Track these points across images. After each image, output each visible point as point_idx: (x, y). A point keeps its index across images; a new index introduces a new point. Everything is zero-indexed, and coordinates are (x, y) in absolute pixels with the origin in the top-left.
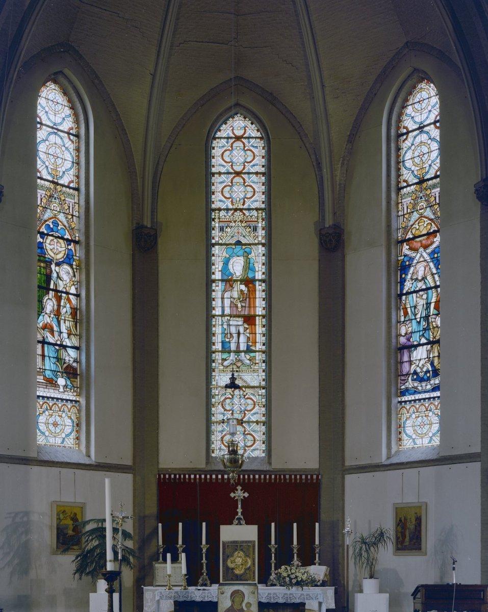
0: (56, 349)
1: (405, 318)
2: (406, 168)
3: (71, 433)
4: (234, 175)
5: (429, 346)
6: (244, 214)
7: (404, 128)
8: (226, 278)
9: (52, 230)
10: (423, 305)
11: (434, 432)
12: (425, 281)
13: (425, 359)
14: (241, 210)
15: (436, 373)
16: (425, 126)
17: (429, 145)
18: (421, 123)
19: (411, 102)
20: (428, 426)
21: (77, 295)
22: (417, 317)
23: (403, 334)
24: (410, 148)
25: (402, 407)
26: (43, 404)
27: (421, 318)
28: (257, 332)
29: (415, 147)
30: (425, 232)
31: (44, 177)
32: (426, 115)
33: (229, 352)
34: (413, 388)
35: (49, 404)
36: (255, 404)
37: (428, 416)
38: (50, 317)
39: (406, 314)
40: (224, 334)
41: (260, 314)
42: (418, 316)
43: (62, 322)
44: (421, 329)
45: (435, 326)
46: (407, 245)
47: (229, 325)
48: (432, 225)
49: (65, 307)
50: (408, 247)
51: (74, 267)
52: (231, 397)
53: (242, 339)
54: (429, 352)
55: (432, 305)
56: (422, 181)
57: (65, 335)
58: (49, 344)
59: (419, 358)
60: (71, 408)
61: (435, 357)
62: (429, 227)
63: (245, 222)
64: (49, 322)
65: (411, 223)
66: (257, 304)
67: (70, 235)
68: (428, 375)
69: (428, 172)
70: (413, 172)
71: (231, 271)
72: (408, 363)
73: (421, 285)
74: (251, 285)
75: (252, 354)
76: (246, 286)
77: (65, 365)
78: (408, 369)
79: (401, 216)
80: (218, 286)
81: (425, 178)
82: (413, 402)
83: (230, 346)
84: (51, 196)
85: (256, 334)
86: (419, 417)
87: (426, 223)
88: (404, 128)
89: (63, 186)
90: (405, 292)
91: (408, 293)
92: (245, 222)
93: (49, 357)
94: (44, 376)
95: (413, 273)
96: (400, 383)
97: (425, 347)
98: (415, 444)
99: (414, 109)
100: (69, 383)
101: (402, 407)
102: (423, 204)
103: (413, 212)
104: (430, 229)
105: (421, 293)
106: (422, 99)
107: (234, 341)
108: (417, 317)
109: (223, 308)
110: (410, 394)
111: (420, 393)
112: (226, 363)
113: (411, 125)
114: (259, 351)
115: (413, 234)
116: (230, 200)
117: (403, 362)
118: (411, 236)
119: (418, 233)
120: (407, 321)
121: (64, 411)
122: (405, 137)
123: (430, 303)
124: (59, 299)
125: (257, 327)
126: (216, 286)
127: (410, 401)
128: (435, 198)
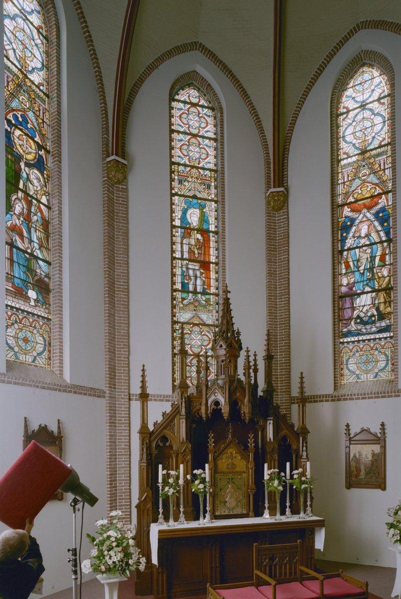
0: (26, 257)
1: (347, 270)
2: (346, 142)
3: (43, 352)
4: (190, 136)
5: (374, 294)
6: (200, 173)
7: (344, 108)
8: (184, 225)
9: (21, 124)
10: (367, 258)
12: (368, 238)
13: (369, 305)
14: (197, 168)
15: (381, 317)
17: (372, 119)
18: (363, 101)
19: (351, 85)
20: (374, 364)
21: (49, 207)
22: (360, 269)
24: (351, 124)
25: (345, 347)
26: (12, 315)
27: (364, 270)
28: (211, 277)
29: (357, 123)
30: (368, 195)
31: (11, 59)
32: (368, 95)
33: (188, 292)
34: (356, 330)
35: (18, 317)
36: (210, 341)
37: (373, 354)
38: (19, 219)
39: (348, 266)
40: (183, 275)
41: (214, 261)
42: (362, 268)
43: (33, 230)
44: (365, 279)
45: (380, 276)
46: (348, 208)
47: (188, 269)
48: (376, 189)
49: (35, 215)
50: (349, 210)
51: (45, 176)
52: (190, 332)
53: (199, 282)
54: (373, 299)
55: (377, 259)
56: (364, 152)
57: (36, 246)
58: (18, 248)
59: (363, 304)
60: (42, 326)
61: (380, 303)
62: (373, 190)
63: (201, 180)
64: (19, 225)
65: (353, 189)
67: (382, 189)
68: (373, 319)
69: (371, 143)
70: (354, 145)
71: (189, 220)
74: (205, 235)
75: (207, 296)
76: (202, 236)
77: (36, 278)
78: (350, 315)
79: (342, 183)
80: (178, 232)
81: (368, 149)
83: (189, 288)
84: (19, 85)
85: (210, 279)
86: (363, 355)
87: (370, 187)
88: (344, 108)
89: (33, 82)
90: (346, 248)
91: (349, 249)
92: (201, 180)
93: (19, 264)
94: (13, 283)
95: (355, 232)
97: (369, 295)
98: (359, 378)
99: (355, 91)
100: (40, 298)
101: (345, 347)
102: (366, 171)
103: (354, 179)
104: (374, 193)
105: (364, 248)
106: (363, 81)
107: (191, 283)
108: (360, 269)
109: (182, 252)
110: (353, 336)
111: (364, 334)
112: (185, 302)
113: (351, 105)
114: (213, 294)
115: (355, 198)
116: (188, 157)
117: (344, 309)
118: (353, 200)
119: (360, 197)
121: (35, 327)
122: (345, 116)
124: (30, 204)
125: (211, 272)
126: (176, 232)
127: (353, 342)
128: (380, 165)
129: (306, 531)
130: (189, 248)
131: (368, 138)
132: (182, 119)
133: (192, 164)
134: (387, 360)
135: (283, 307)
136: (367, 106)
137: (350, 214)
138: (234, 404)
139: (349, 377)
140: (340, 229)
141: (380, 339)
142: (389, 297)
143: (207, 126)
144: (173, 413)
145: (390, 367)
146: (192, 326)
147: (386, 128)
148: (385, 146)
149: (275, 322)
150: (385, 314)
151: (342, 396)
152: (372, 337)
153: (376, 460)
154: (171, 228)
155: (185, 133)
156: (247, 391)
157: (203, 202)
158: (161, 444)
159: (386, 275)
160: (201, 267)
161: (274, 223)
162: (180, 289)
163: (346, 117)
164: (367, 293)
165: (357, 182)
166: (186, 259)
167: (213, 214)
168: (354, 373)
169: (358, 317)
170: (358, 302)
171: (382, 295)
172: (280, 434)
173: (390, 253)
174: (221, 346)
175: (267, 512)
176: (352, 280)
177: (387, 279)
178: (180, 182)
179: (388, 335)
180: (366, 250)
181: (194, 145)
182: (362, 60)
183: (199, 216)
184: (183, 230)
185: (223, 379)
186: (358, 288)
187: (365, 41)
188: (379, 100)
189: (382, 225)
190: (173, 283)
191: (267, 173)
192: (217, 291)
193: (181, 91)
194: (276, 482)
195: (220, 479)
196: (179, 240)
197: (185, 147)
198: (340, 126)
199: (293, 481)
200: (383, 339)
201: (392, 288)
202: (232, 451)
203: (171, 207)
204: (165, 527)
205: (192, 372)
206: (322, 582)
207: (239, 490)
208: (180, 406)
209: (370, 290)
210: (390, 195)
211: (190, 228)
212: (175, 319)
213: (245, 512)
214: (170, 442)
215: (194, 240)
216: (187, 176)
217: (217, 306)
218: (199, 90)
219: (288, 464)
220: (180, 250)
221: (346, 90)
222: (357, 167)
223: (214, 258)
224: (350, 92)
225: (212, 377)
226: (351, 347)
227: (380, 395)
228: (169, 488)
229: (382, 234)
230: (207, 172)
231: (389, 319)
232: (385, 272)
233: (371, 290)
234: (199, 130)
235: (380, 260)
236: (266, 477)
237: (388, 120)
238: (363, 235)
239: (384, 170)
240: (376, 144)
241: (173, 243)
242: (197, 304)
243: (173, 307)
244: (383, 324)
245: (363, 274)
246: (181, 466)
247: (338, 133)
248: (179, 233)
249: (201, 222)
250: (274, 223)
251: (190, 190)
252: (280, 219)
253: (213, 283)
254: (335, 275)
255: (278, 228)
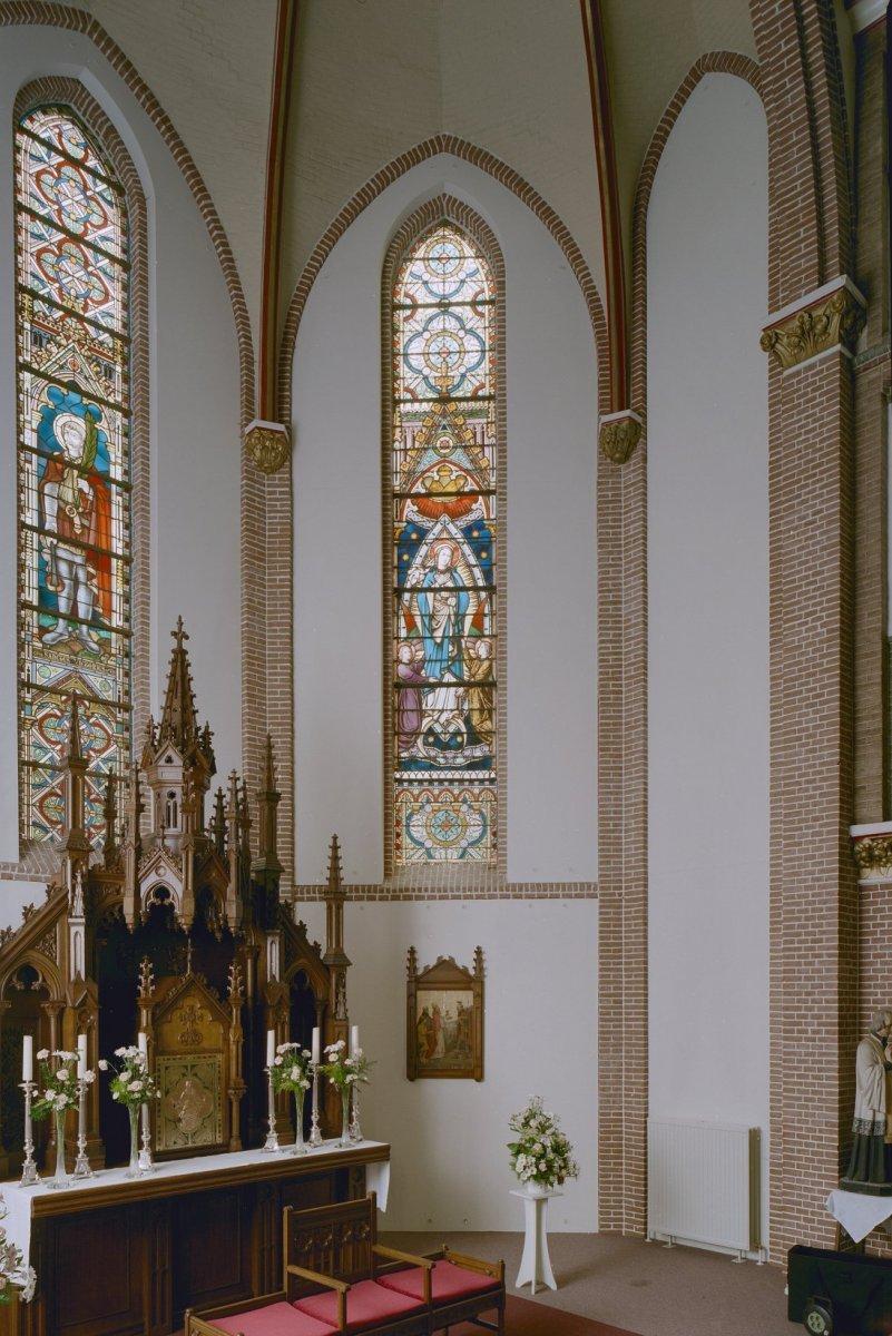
1: (409, 631)
5: (461, 690)
6: (87, 333)
7: (407, 295)
8: (47, 450)
11: (471, 840)
13: (452, 711)
14: (81, 319)
15: (475, 738)
16: (450, 304)
19: (420, 253)
20: (459, 830)
23: (405, 660)
25: (404, 790)
27: (443, 637)
32: (453, 289)
33: (57, 615)
34: (426, 758)
36: (109, 740)
39: (411, 625)
41: (120, 552)
42: (439, 633)
47: (56, 558)
48: (467, 480)
50: (416, 508)
52: (59, 714)
54: (460, 700)
55: (468, 621)
56: (444, 399)
61: (472, 710)
62: (462, 482)
65: (422, 467)
66: (114, 532)
67: (477, 483)
68: (459, 739)
69: (459, 386)
71: (60, 439)
72: (415, 713)
73: (442, 580)
75: (104, 634)
79: (400, 450)
80: (31, 462)
81: (453, 395)
82: (467, 783)
85: (110, 592)
87: (455, 474)
90: (408, 586)
91: (414, 590)
95: (426, 556)
96: (399, 747)
97: (453, 689)
98: (430, 856)
101: (404, 790)
102: (446, 438)
103: (425, 449)
104: (463, 486)
106: (445, 256)
107: (64, 594)
110: (421, 769)
112: (48, 637)
114: (116, 631)
118: (423, 491)
119: (436, 488)
120: (413, 638)
123: (464, 615)
125: (114, 578)
126: (26, 461)
127: (421, 782)
129: (347, 1174)
130: (59, 508)
131: (452, 374)
132: (43, 186)
133: (68, 305)
134: (485, 826)
135: (279, 687)
136: (451, 309)
137: (417, 518)
138: (205, 896)
139: (412, 852)
140: (399, 545)
141: (471, 781)
142: (488, 699)
143: (104, 225)
144: (50, 911)
145: (488, 840)
146: (64, 698)
147: (486, 365)
148: (483, 398)
149: (261, 717)
150: (481, 733)
151: (401, 891)
152: (457, 775)
153: (466, 1022)
154: (18, 449)
155: (47, 221)
156: (233, 869)
157: (95, 406)
158: (19, 986)
159: (484, 656)
160: (88, 559)
161: (260, 497)
162: (35, 603)
163: (411, 316)
164: (448, 685)
165: (430, 457)
166: (50, 534)
167: (119, 440)
168: (422, 844)
169: (431, 732)
170: (430, 703)
171: (476, 693)
172: (292, 966)
173: (492, 614)
174: (169, 760)
175: (272, 1137)
176: (420, 655)
177: (486, 664)
178: (37, 340)
179: (487, 776)
180: (448, 598)
181: (74, 260)
182: (443, 214)
183: (84, 436)
184: (44, 461)
185: (176, 837)
186: (431, 673)
187: (443, 176)
188: (474, 304)
189: (477, 554)
190: (21, 588)
191: (247, 381)
192: (126, 626)
193: (39, 113)
194: (296, 1071)
195: (167, 1068)
196: (33, 482)
197: (49, 258)
198: (398, 331)
199: (328, 1068)
200: (476, 783)
201: (493, 684)
202: (195, 1002)
203: (18, 398)
204: (43, 1189)
205: (94, 815)
206: (429, 1271)
207: (206, 1091)
208: (70, 896)
209: (454, 680)
210: (493, 499)
211: (60, 460)
212: (24, 676)
213: (219, 1140)
214: (44, 980)
215: (71, 491)
216: (53, 331)
217: (126, 661)
218: (84, 130)
219: (316, 1032)
220: (35, 507)
221: (411, 260)
222: (432, 426)
223: (121, 545)
224: (416, 267)
225: (149, 824)
226: (416, 792)
227: (450, 894)
228: (57, 1094)
229: (477, 572)
230: (105, 337)
231: (489, 745)
232: (482, 649)
233: (455, 680)
234: (86, 228)
235: (473, 624)
236: (270, 1061)
237: (490, 350)
238: (441, 567)
239: (483, 446)
240: (466, 389)
241: (21, 488)
242: (77, 648)
243: (21, 647)
244: (478, 753)
245: (440, 646)
246: (82, 1039)
247: (394, 344)
248: (34, 464)
249: (90, 452)
250: (260, 497)
251: (62, 367)
252: (274, 493)
253: (116, 603)
254: (388, 639)
255: (270, 512)
